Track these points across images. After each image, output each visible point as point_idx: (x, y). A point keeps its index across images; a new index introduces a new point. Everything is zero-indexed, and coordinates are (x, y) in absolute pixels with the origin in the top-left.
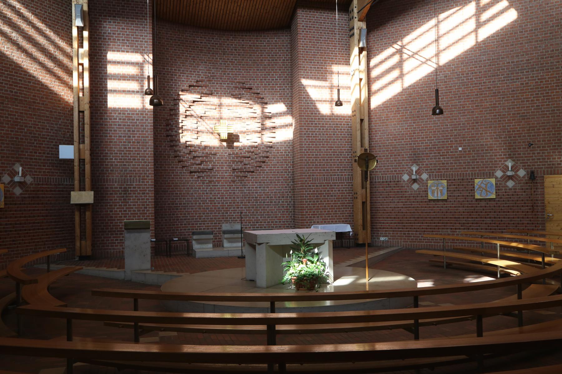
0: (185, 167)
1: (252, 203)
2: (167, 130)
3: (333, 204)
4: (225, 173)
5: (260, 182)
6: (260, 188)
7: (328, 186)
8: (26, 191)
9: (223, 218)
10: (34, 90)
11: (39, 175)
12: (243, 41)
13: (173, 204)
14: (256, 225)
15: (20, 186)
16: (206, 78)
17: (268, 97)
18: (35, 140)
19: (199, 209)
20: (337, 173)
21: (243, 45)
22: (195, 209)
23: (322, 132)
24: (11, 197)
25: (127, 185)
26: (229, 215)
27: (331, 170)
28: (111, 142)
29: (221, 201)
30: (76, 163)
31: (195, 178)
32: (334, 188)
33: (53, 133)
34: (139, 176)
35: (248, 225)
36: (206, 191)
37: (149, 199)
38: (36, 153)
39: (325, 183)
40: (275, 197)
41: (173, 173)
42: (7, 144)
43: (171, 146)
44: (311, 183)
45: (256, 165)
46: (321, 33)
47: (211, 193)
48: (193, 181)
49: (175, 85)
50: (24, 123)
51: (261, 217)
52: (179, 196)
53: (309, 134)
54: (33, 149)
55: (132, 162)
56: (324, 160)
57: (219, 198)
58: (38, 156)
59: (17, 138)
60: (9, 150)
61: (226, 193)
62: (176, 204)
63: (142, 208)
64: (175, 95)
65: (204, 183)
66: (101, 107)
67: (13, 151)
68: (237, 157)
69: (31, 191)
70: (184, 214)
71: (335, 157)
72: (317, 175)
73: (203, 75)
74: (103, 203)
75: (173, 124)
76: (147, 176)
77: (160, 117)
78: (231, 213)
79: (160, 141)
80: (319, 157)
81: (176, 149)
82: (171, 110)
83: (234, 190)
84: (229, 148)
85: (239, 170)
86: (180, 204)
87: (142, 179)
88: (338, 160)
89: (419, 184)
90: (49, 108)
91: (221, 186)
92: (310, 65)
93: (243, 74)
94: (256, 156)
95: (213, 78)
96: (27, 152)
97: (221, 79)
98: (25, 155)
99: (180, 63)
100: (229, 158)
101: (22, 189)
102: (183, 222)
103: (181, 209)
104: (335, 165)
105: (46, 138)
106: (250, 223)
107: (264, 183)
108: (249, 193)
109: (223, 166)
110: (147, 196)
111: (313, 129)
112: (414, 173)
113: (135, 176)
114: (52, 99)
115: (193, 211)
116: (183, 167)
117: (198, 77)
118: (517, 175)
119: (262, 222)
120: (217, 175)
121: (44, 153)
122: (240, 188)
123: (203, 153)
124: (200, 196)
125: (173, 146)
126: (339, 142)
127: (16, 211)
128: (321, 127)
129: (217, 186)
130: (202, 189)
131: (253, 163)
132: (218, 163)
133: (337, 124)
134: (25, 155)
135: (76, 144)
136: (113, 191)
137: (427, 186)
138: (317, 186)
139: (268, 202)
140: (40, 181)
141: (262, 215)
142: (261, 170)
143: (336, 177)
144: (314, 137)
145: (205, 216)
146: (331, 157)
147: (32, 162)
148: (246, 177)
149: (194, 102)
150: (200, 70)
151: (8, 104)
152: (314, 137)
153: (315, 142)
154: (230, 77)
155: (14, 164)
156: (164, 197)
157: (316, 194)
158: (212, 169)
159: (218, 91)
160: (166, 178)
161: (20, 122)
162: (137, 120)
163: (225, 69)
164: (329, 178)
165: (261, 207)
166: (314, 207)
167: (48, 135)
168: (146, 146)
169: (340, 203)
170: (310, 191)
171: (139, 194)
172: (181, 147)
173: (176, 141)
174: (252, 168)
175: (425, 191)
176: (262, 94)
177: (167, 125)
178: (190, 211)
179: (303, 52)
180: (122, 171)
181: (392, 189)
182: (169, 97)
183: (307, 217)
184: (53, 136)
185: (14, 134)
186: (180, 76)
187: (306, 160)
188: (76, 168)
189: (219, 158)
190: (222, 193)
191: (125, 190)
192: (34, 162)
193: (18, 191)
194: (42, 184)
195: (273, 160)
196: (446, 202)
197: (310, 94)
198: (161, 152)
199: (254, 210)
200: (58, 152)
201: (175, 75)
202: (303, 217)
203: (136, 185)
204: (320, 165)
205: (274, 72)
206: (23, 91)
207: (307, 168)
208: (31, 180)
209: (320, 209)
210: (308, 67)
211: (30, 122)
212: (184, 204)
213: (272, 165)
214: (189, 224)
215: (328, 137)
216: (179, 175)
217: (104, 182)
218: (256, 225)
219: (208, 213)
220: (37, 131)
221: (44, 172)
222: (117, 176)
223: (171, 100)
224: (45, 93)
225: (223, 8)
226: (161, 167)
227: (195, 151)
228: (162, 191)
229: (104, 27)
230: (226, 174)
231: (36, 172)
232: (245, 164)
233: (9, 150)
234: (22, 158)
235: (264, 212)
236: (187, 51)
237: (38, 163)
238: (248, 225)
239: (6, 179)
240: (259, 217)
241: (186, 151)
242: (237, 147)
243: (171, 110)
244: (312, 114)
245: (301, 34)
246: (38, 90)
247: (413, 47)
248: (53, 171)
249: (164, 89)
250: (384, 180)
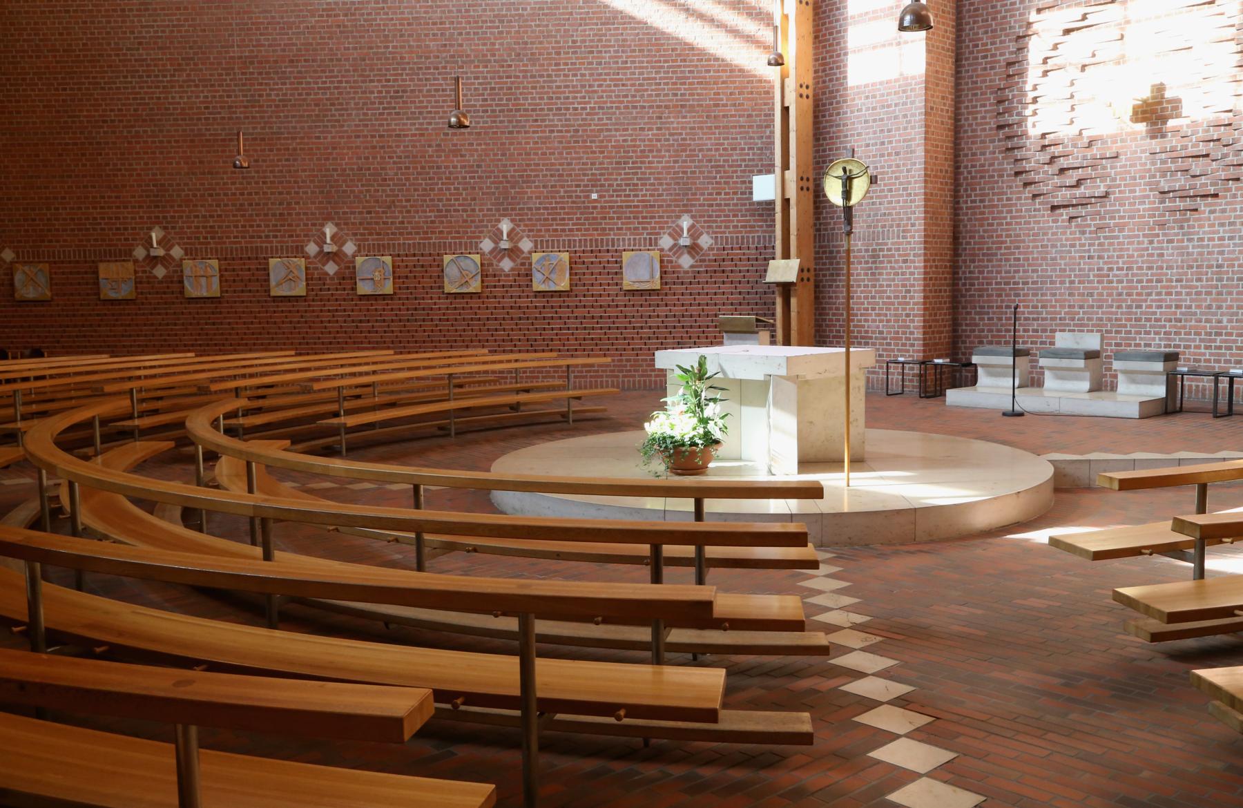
0: (1039, 195)
1: (1207, 280)
4: (1140, 203)
6: (1231, 238)
8: (701, 261)
10: (715, 83)
11: (725, 232)
13: (1008, 283)
14: (1215, 341)
15: (689, 253)
18: (718, 172)
22: (1061, 294)
24: (674, 272)
26: (1146, 313)
30: (778, 208)
31: (1063, 221)
34: (898, 226)
35: (1194, 340)
36: (1089, 251)
37: (914, 274)
38: (719, 194)
41: (1011, 212)
42: (667, 184)
43: (1008, 149)
45: (1223, 175)
47: (1100, 257)
48: (1057, 227)
51: (1230, 321)
52: (1024, 266)
55: (886, 196)
57: (1122, 269)
58: (724, 199)
59: (685, 173)
60: (671, 194)
61: (1139, 256)
62: (1015, 283)
63: (901, 291)
64: (1020, 27)
65: (1084, 233)
66: (838, 91)
68: (1174, 159)
70: (1033, 307)
75: (1014, 96)
76: (913, 225)
77: (984, 85)
78: (1150, 307)
79: (982, 142)
82: (1010, 64)
83: (1162, 248)
84: (1153, 137)
85: (1178, 194)
86: (1023, 283)
87: (904, 231)
90: (745, 110)
91: (1129, 237)
94: (1225, 150)
96: (703, 194)
100: (1153, 164)
102: (1029, 325)
105: (740, 166)
106: (1199, 334)
108: (1201, 254)
109: (1135, 185)
110: (910, 267)
112: (505, 237)
113: (892, 226)
115: (1056, 301)
116: (1035, 196)
118: (171, 257)
119: (1231, 334)
120: (1119, 211)
121: (735, 193)
122: (1178, 241)
123: (1085, 158)
125: (1013, 149)
129: (1117, 237)
130: (1078, 248)
132: (1122, 179)
134: (699, 200)
135: (778, 170)
137: (530, 264)
140: (727, 244)
145: (1084, 313)
147: (713, 211)
148: (1196, 210)
149: (1067, 32)
151: (669, 117)
155: (679, 217)
156: (988, 267)
158: (1106, 195)
160: (992, 225)
161: (690, 145)
165: (1230, 293)
168: (910, 159)
171: (897, 262)
172: (1030, 150)
174: (1212, 185)
175: (527, 275)
177: (1000, 102)
178: (1047, 301)
180: (869, 216)
184: (753, 160)
185: (679, 167)
189: (1125, 166)
191: (875, 252)
192: (716, 211)
193: (686, 262)
196: (392, 299)
198: (982, 165)
199: (1212, 300)
203: (893, 244)
206: (696, 89)
208: (711, 241)
211: (708, 142)
216: (1025, 217)
217: (828, 241)
218: (1215, 341)
220: (721, 155)
222: (861, 227)
223: (1010, 41)
224: (737, 84)
226: (981, 201)
230: (1141, 207)
231: (720, 227)
232: (1193, 177)
233: (671, 194)
234: (694, 205)
237: (724, 210)
238: (1194, 340)
240: (1225, 319)
242: (1176, 131)
243: (1010, 64)
246: (723, 82)
248: (752, 223)
249: (994, 19)
250: (577, 249)
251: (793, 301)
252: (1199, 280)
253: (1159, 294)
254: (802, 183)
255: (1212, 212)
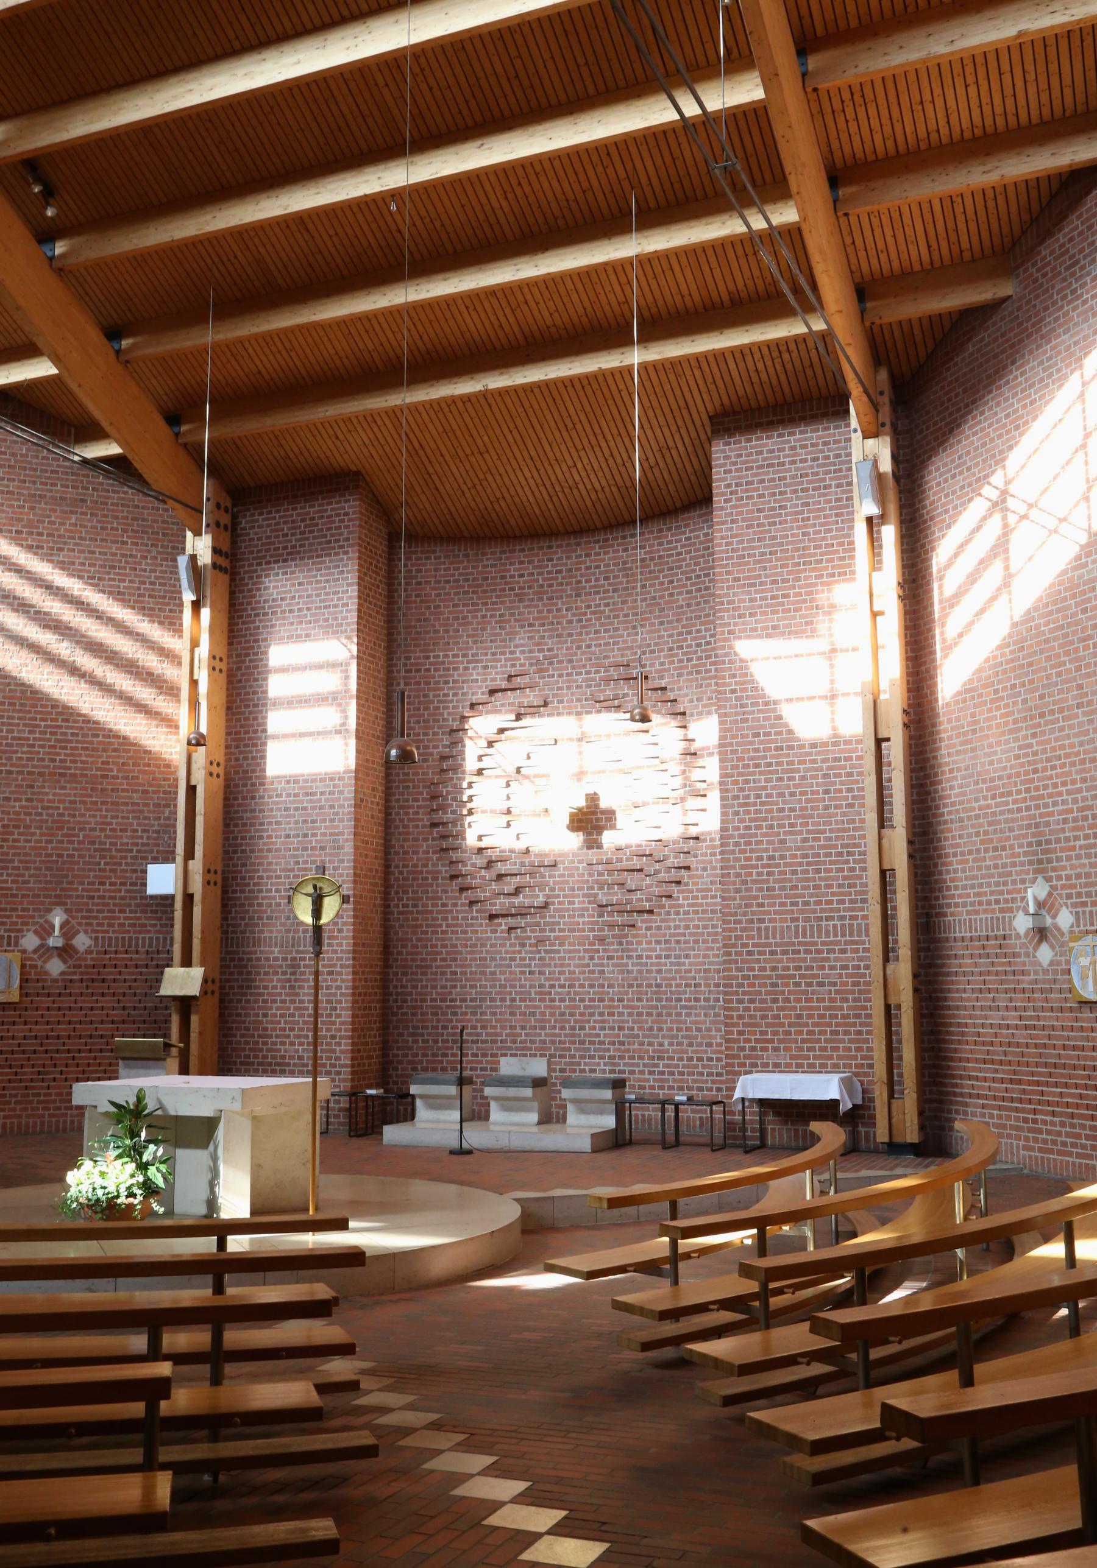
2: (433, 810)
3: (826, 1008)
5: (667, 942)
6: (667, 957)
7: (807, 952)
8: (75, 966)
9: (574, 1042)
12: (625, 550)
13: (443, 1000)
15: (60, 956)
16: (531, 665)
17: (686, 695)
19: (511, 1014)
20: (838, 910)
21: (625, 563)
22: (502, 1014)
23: (788, 787)
24: (38, 981)
25: (298, 952)
26: (590, 1035)
27: (819, 903)
28: (269, 850)
29: (569, 993)
30: (178, 905)
32: (828, 960)
33: (148, 838)
35: (638, 1065)
39: (800, 943)
40: (708, 985)
41: (446, 919)
42: (35, 869)
43: (442, 850)
44: (755, 945)
45: (656, 891)
46: (781, 493)
47: (541, 973)
49: (455, 695)
50: (79, 823)
51: (671, 1044)
53: (748, 797)
54: (95, 877)
56: (794, 872)
58: (109, 891)
64: (454, 720)
66: (253, 771)
67: (51, 882)
68: (611, 872)
69: (86, 966)
71: (832, 862)
72: (771, 921)
73: (526, 658)
74: (251, 994)
75: (448, 793)
80: (778, 865)
81: (454, 856)
82: (443, 758)
84: (589, 848)
85: (616, 908)
88: (842, 870)
89: (1052, 947)
90: (140, 785)
91: (570, 951)
92: (749, 593)
93: (625, 642)
95: (551, 663)
97: (570, 661)
98: (76, 890)
99: (468, 636)
100: (590, 875)
101: (65, 961)
103: (466, 1014)
104: (830, 886)
105: (131, 851)
107: (678, 942)
111: (759, 781)
114: (149, 765)
116: (472, 903)
117: (513, 666)
120: (558, 923)
121: (123, 884)
123: (522, 864)
124: (514, 979)
126: (843, 814)
127: (48, 1009)
128: (784, 771)
129: (558, 952)
131: (651, 886)
133: (836, 759)
134: (76, 890)
135: (180, 859)
136: (270, 966)
138: (773, 953)
139: (689, 1000)
140: (110, 945)
141: (673, 1037)
142: (671, 906)
143: (835, 926)
144: (762, 804)
146: (818, 863)
150: (516, 646)
151: (43, 787)
152: (762, 804)
153: (765, 819)
154: (594, 653)
155: (49, 911)
157: (769, 977)
158: (545, 906)
159: (563, 695)
162: (322, 793)
163: (581, 634)
164: (812, 926)
165: (669, 1015)
166: (763, 1017)
167: (137, 844)
168: (337, 855)
169: (849, 1008)
170: (752, 969)
173: (455, 837)
174: (648, 900)
176: (672, 690)
179: (728, 558)
181: (993, 964)
182: (440, 727)
183: (743, 1049)
184: (147, 845)
186: (466, 669)
187: (738, 875)
188: (178, 915)
189: (563, 876)
190: (570, 972)
193: (55, 967)
194: (116, 952)
195: (702, 877)
197: (757, 677)
198: (416, 866)
200: (145, 878)
201: (455, 669)
202: (732, 1049)
204: (781, 888)
205: (701, 624)
207: (742, 898)
209: (782, 1025)
210: (744, 601)
212: (472, 1000)
213: (698, 890)
214: (485, 1055)
215: (807, 801)
219: (535, 1028)
221: (122, 925)
222: (278, 931)
225: (539, 481)
226: (415, 906)
227: (503, 861)
228: (417, 967)
229: (266, 588)
230: (581, 920)
231: (102, 925)
232: (629, 891)
234: (70, 897)
235: (679, 1030)
236: (486, 604)
239: (30, 941)
241: (480, 861)
243: (443, 758)
244: (758, 735)
245: (722, 509)
246: (115, 750)
247: (1023, 490)
251: (194, 1019)
252: (640, 1000)
253: (601, 1014)
254: (208, 877)
255: (648, 929)
